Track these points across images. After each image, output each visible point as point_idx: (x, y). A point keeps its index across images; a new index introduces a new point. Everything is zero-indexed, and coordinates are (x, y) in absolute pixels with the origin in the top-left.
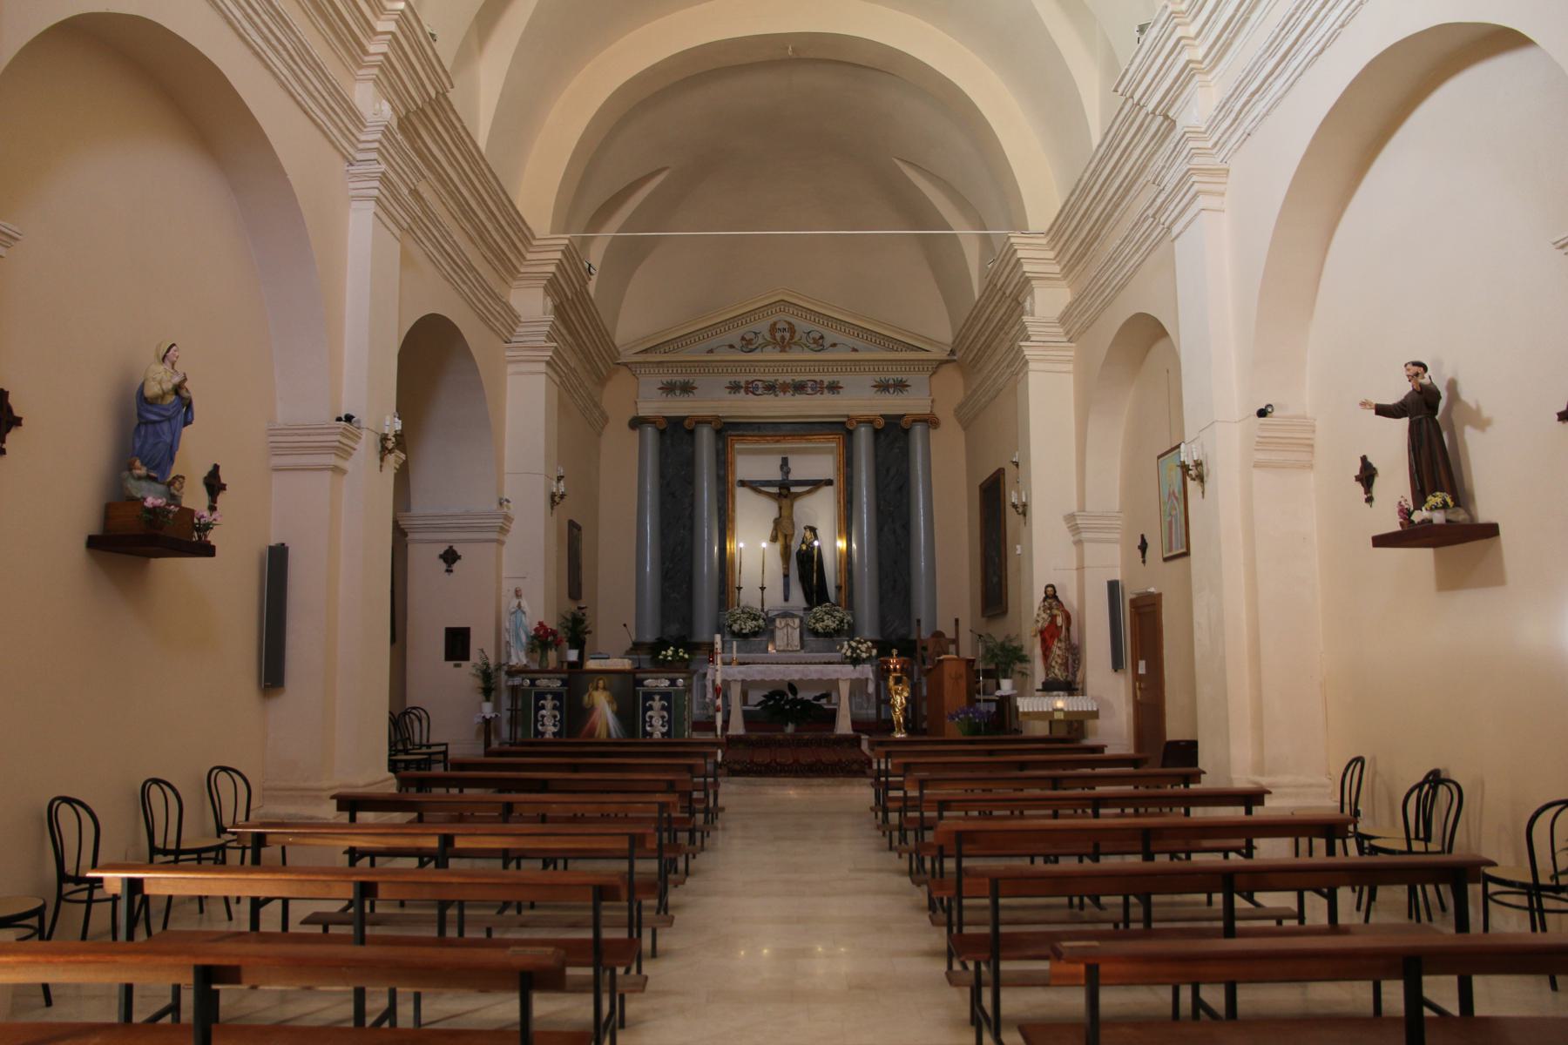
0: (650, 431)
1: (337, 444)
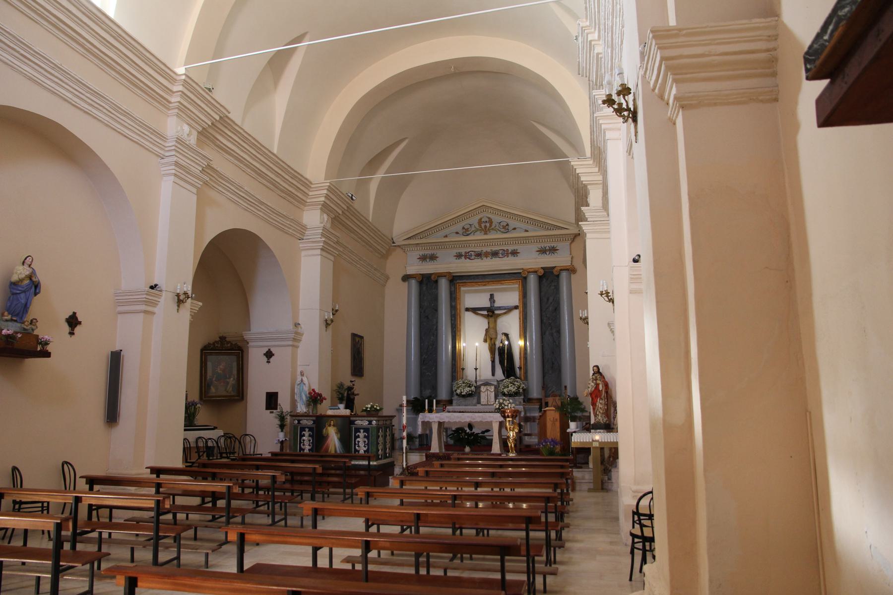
0: (413, 282)
1: (144, 299)
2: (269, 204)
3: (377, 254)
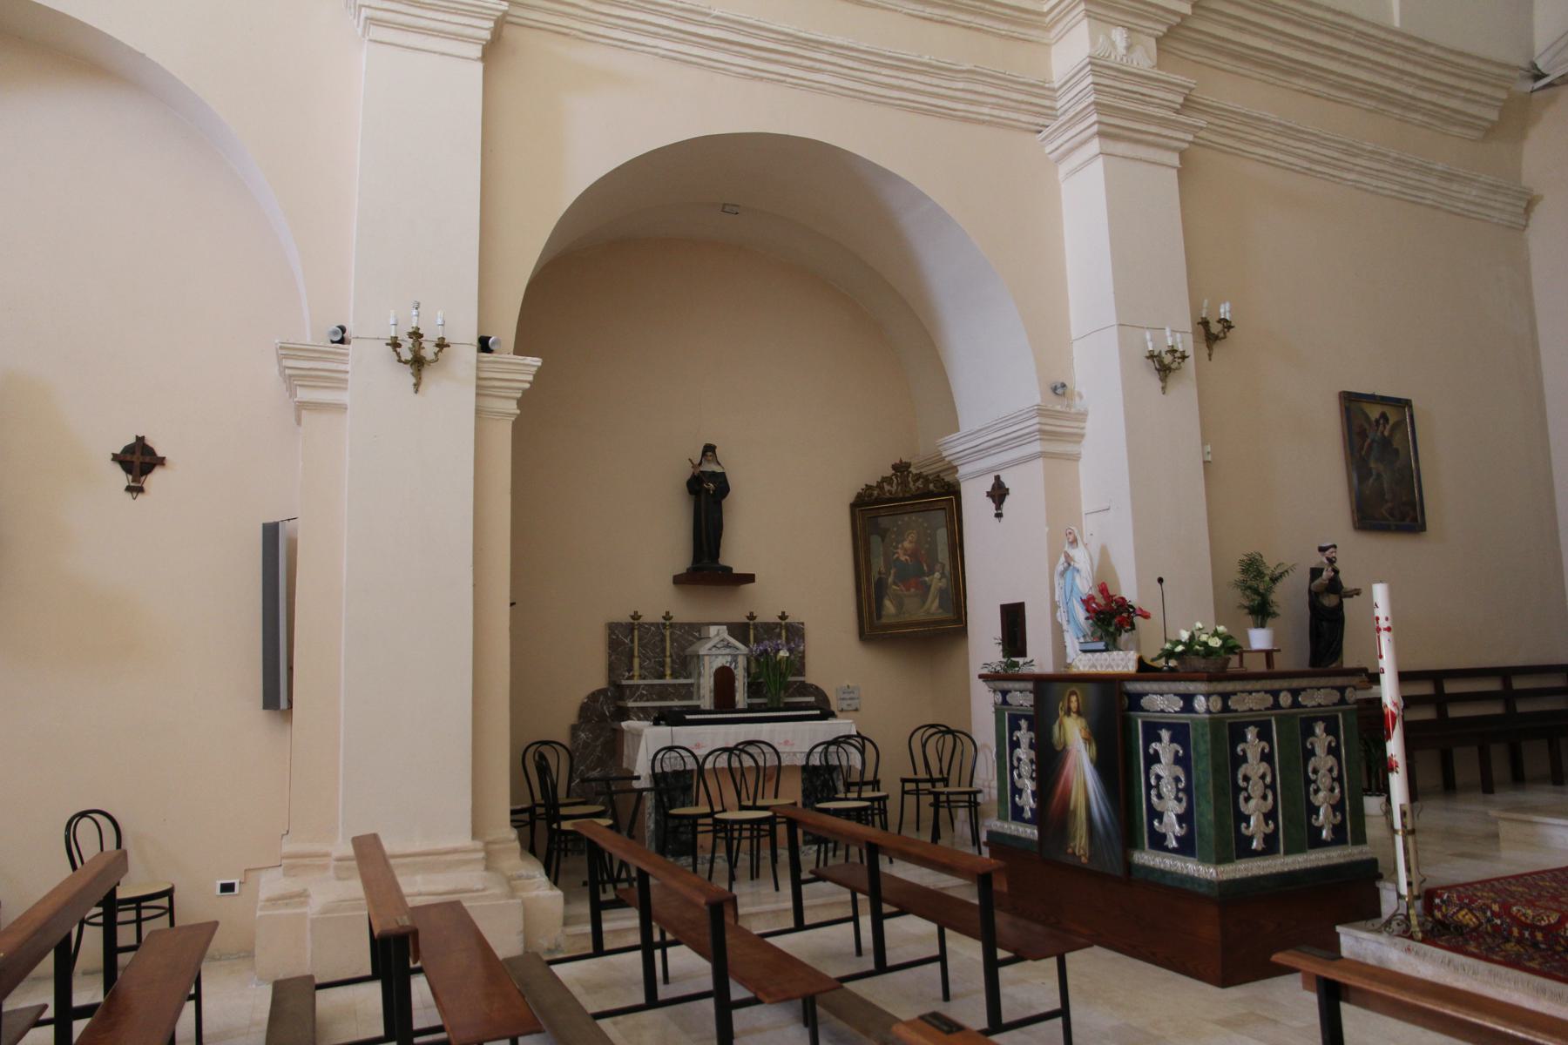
2: (838, 40)
3: (1456, 130)
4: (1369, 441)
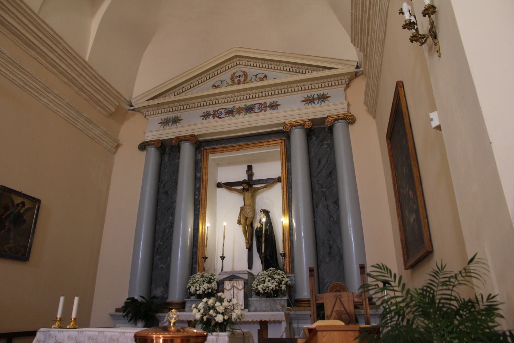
0: (152, 151)
4: (9, 212)
